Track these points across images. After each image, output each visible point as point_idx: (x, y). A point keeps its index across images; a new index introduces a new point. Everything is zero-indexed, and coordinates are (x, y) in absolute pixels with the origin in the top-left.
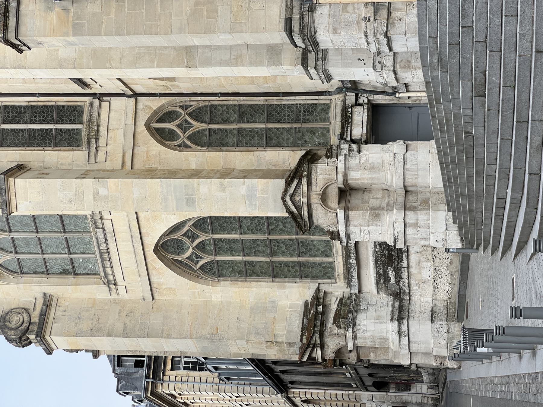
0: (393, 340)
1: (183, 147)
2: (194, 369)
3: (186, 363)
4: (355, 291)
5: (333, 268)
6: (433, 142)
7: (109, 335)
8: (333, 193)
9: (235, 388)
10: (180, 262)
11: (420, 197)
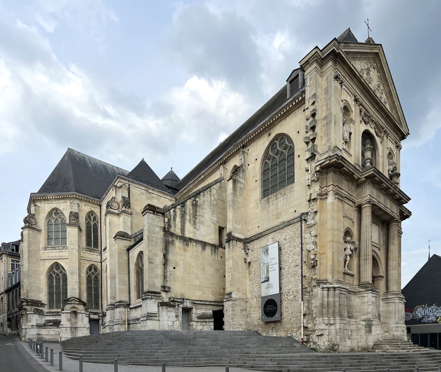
0: (31, 324)
1: (87, 273)
2: (12, 266)
3: (14, 264)
4: (45, 314)
6: (89, 335)
8: (75, 310)
9: (6, 278)
10: (53, 268)
11: (74, 331)
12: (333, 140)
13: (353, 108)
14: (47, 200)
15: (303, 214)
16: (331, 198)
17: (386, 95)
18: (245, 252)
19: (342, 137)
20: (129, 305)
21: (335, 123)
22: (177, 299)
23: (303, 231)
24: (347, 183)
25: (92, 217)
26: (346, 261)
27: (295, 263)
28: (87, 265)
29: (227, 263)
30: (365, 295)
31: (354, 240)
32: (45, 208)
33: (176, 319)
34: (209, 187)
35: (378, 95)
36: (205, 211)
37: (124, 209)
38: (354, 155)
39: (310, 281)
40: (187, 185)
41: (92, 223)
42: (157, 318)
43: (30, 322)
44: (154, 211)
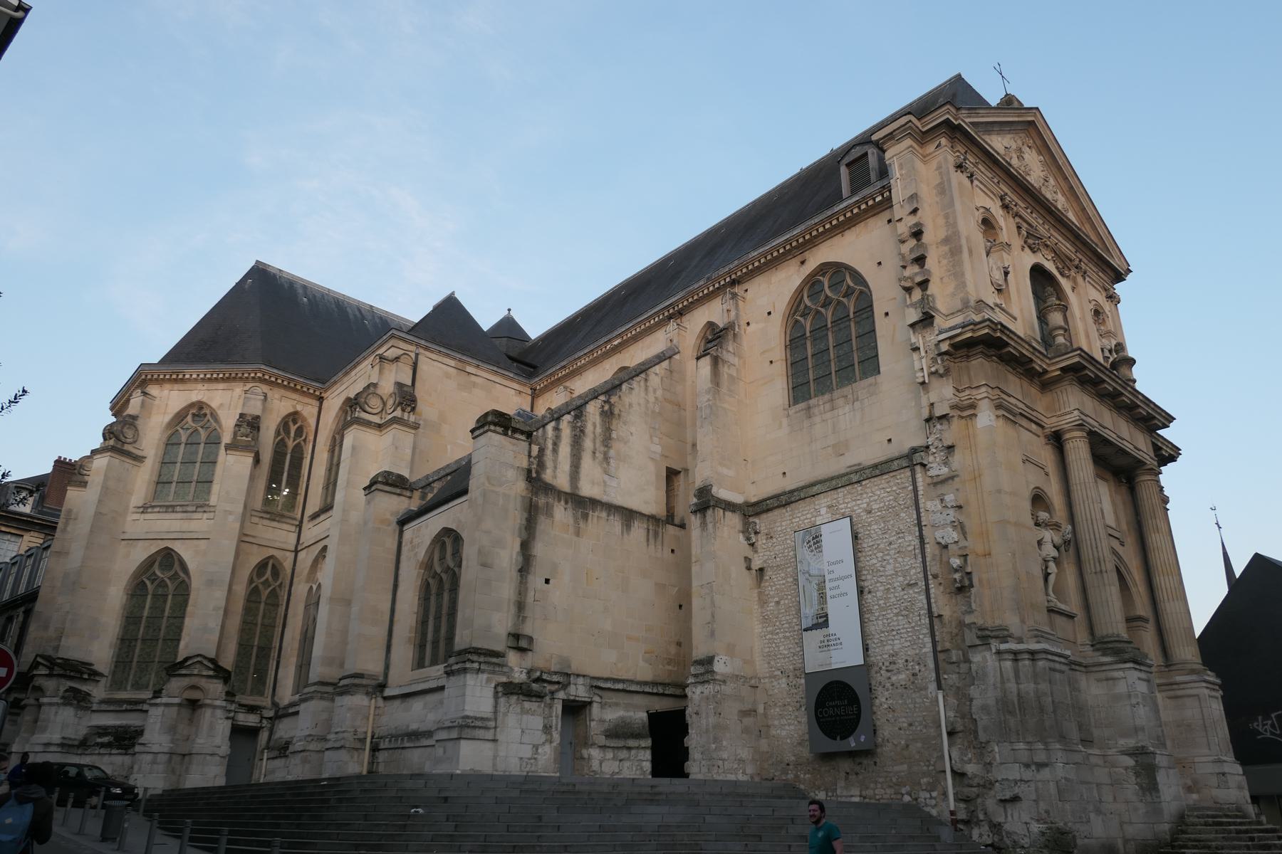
1: (251, 581)
4: (95, 707)
5: (119, 689)
7: (100, 501)
12: (970, 288)
13: (1002, 222)
14: (183, 381)
15: (914, 450)
16: (986, 417)
17: (1064, 194)
18: (748, 539)
19: (990, 279)
20: (382, 686)
21: (970, 252)
22: (550, 673)
23: (920, 493)
24: (1017, 380)
25: (293, 429)
26: (1046, 576)
27: (904, 576)
28: (255, 560)
29: (695, 569)
30: (1116, 674)
31: (1056, 519)
32: (170, 400)
33: (544, 737)
34: (643, 369)
35: (1049, 196)
36: (633, 429)
37: (398, 413)
38: (1020, 315)
39: (955, 631)
40: (571, 359)
41: (291, 444)
42: (489, 735)
43: (44, 730)
44: (506, 428)
